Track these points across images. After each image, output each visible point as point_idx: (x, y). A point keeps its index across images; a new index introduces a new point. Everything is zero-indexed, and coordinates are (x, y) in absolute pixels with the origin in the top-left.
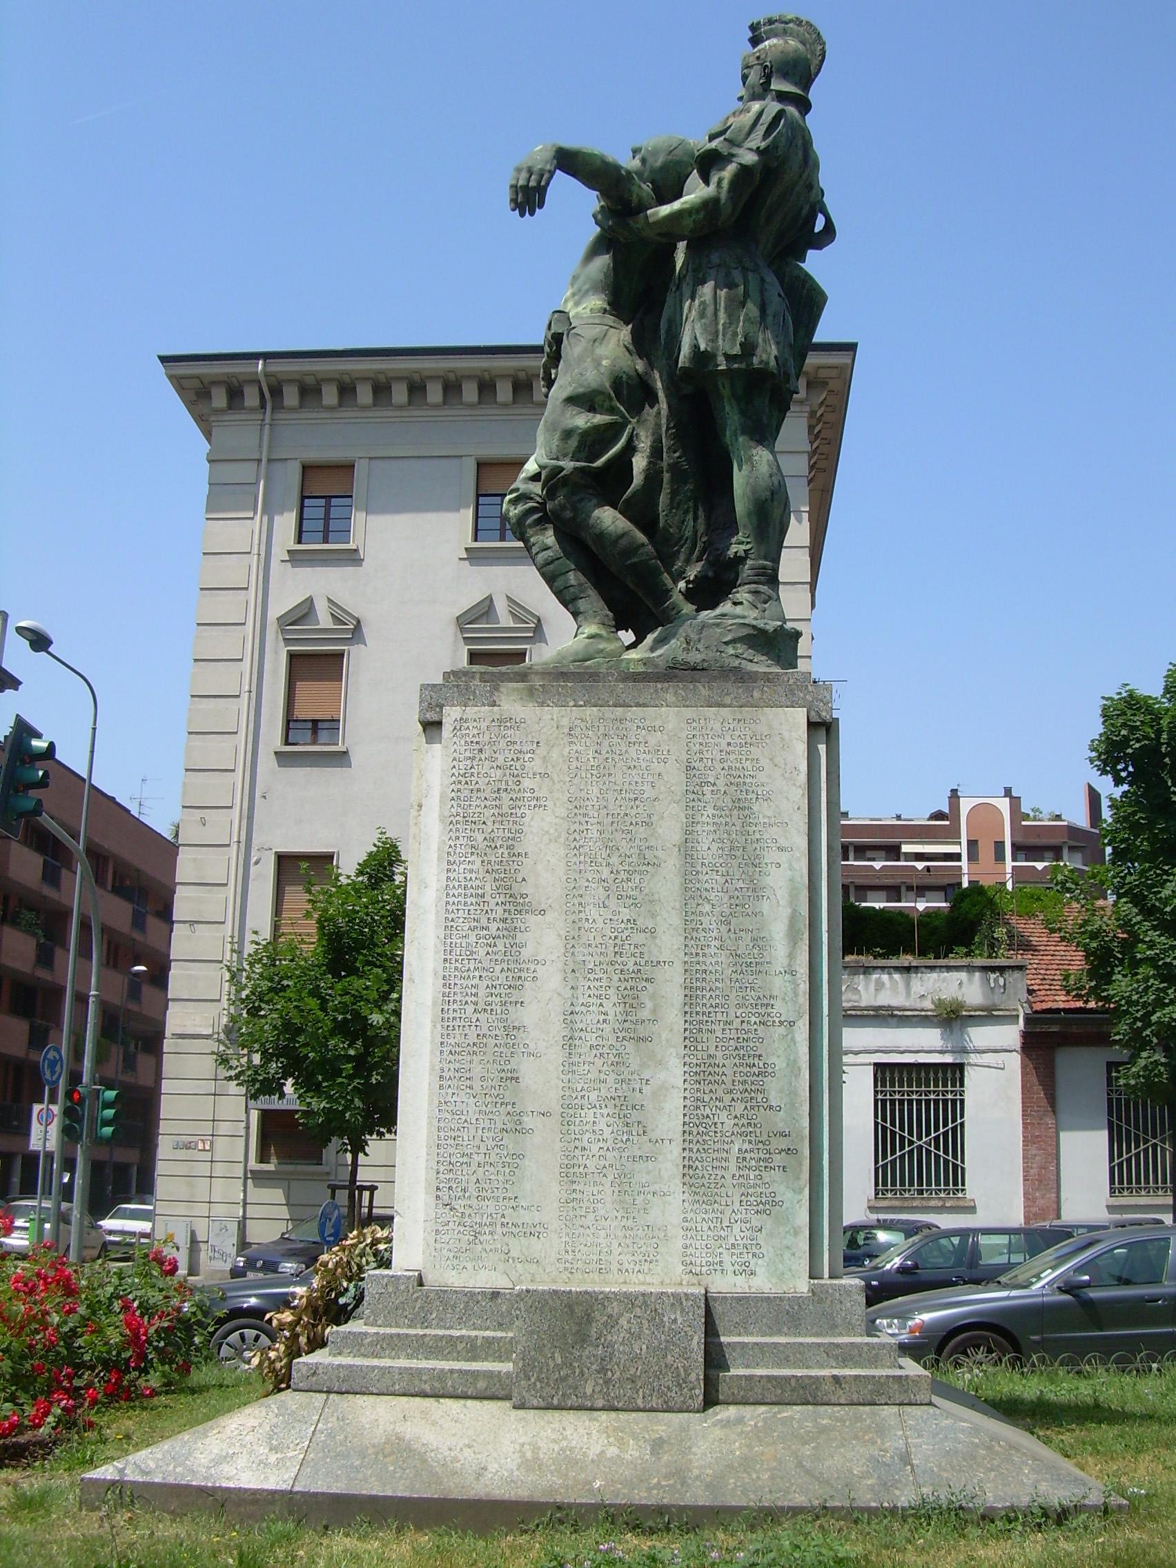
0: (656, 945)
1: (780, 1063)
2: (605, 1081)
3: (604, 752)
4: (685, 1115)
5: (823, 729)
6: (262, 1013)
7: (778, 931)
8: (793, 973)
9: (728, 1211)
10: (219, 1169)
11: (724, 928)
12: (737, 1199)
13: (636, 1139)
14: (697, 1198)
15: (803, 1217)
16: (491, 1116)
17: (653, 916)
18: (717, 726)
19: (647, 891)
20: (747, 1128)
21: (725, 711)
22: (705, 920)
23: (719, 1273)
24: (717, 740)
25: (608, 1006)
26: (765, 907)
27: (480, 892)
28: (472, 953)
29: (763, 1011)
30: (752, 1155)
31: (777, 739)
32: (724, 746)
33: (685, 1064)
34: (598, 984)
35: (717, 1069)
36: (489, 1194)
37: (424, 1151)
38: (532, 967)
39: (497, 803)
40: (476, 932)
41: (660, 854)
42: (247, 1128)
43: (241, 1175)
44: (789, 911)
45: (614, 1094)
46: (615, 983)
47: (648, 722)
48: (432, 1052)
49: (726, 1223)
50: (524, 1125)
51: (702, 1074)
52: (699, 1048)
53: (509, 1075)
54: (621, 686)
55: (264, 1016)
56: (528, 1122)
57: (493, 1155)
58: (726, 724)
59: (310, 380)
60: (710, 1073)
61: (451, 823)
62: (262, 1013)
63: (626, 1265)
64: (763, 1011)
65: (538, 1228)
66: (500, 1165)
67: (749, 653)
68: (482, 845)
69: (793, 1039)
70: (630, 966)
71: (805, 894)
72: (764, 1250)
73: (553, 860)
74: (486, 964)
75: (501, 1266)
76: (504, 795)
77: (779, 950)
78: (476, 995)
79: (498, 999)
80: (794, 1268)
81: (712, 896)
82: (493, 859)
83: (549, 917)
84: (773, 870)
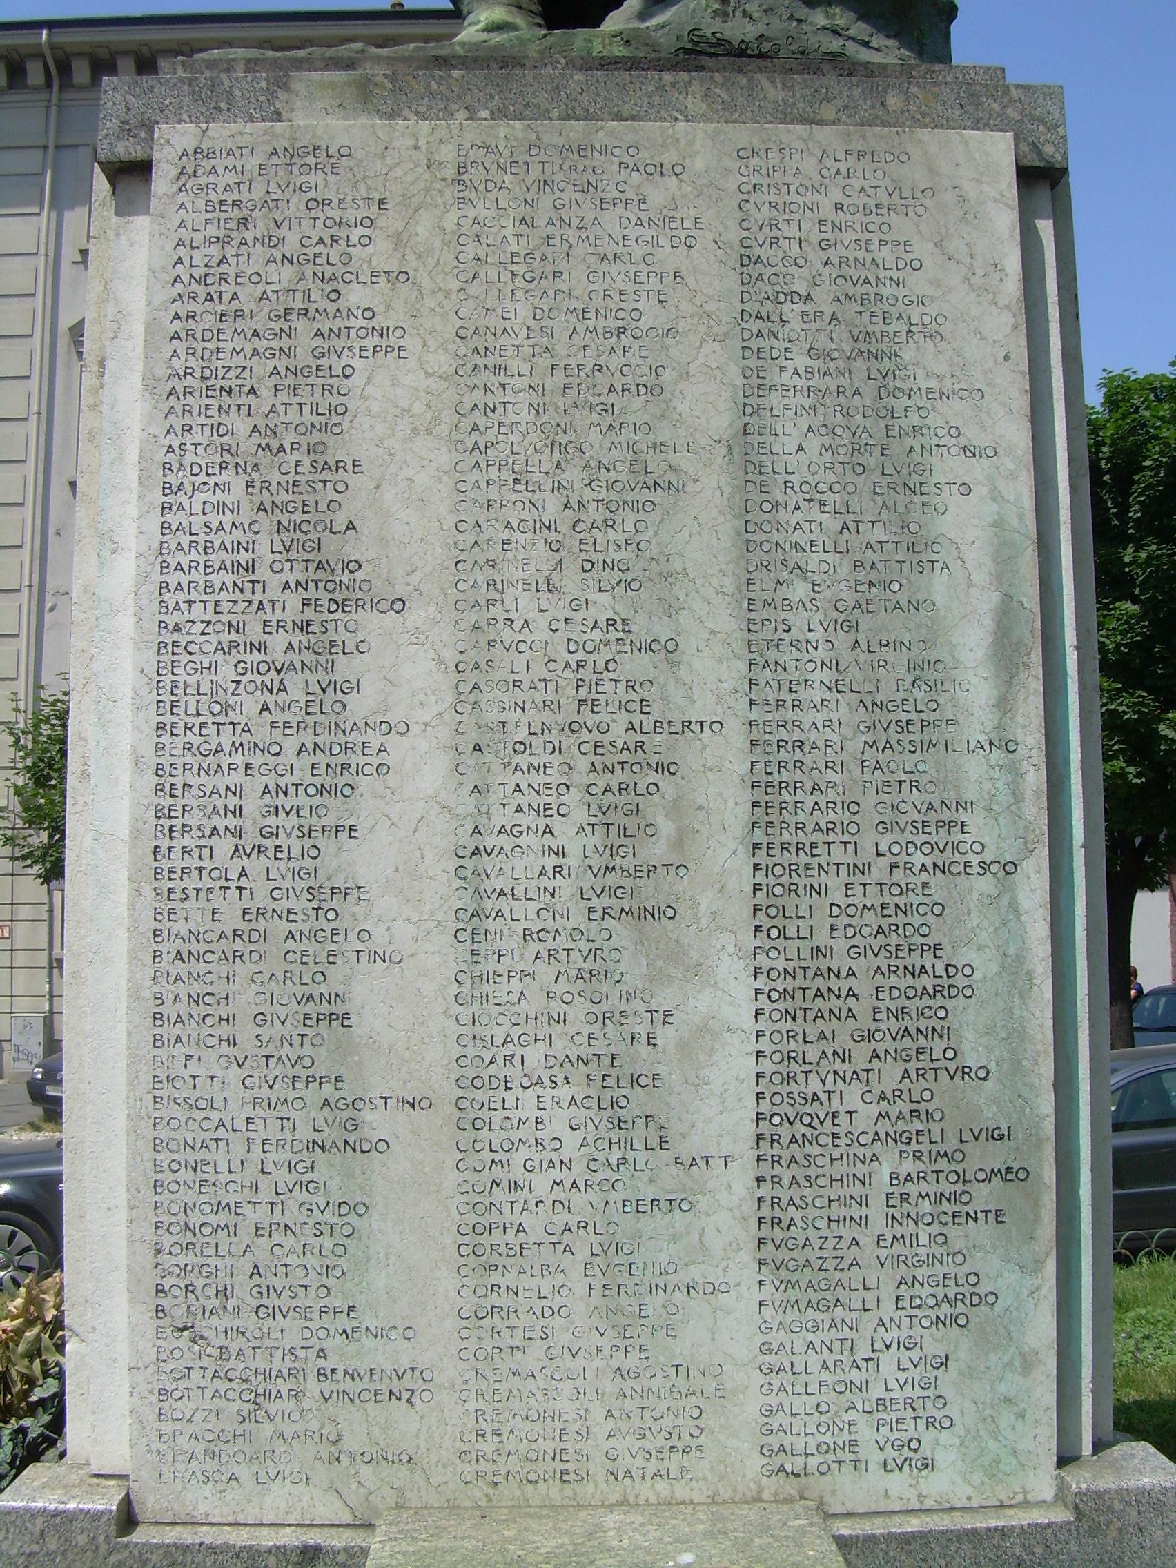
0: (678, 680)
1: (983, 963)
2: (562, 1020)
3: (541, 222)
4: (759, 1096)
5: (1041, 180)
6: (53, 782)
7: (970, 645)
8: (1009, 747)
9: (868, 1323)
10: (21, 959)
11: (842, 640)
12: (888, 1292)
13: (641, 1157)
14: (793, 1295)
15: (1042, 1328)
16: (282, 1111)
17: (671, 610)
18: (810, 166)
19: (653, 550)
20: (911, 1123)
21: (824, 134)
22: (798, 620)
23: (848, 1468)
24: (810, 198)
25: (565, 834)
26: (939, 586)
27: (244, 557)
28: (226, 708)
29: (940, 837)
30: (924, 1187)
31: (949, 197)
32: (827, 211)
33: (757, 972)
34: (537, 779)
35: (834, 983)
36: (285, 1302)
37: (122, 1196)
38: (375, 739)
39: (285, 342)
40: (235, 656)
41: (684, 461)
42: (51, 911)
43: (45, 964)
44: (996, 597)
45: (585, 1051)
46: (581, 775)
47: (645, 155)
48: (133, 957)
49: (863, 1351)
50: (366, 1132)
51: (799, 996)
52: (792, 932)
53: (325, 1008)
54: (579, 76)
55: (54, 787)
56: (376, 1122)
57: (292, 1205)
58: (829, 162)
59: (103, 53)
60: (819, 994)
61: (171, 393)
62: (53, 782)
63: (626, 1462)
64: (940, 837)
65: (408, 1381)
66: (309, 1230)
67: (860, 29)
68: (248, 445)
69: (1014, 907)
70: (618, 733)
71: (1029, 557)
72: (952, 1410)
73: (422, 478)
74: (262, 735)
75: (321, 1474)
76: (300, 324)
77: (976, 690)
78: (238, 812)
79: (293, 820)
80: (1022, 1446)
81: (812, 561)
82: (275, 477)
83: (415, 616)
84: (953, 499)
